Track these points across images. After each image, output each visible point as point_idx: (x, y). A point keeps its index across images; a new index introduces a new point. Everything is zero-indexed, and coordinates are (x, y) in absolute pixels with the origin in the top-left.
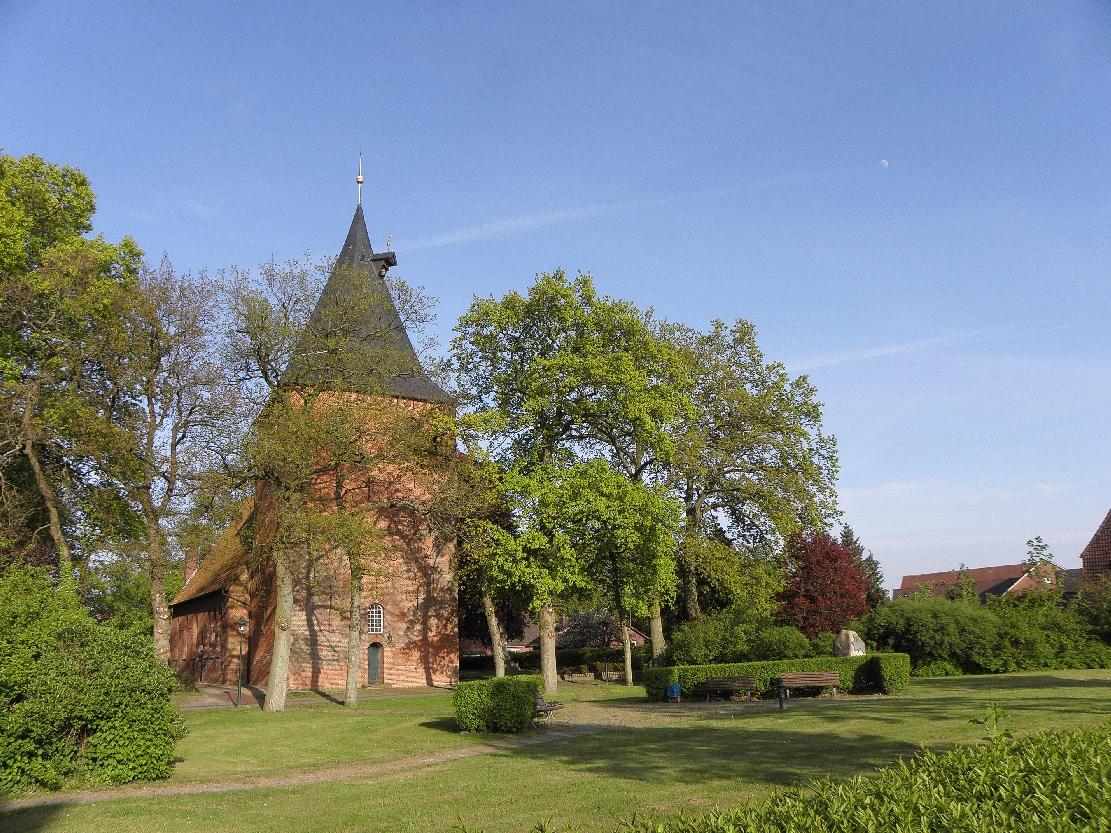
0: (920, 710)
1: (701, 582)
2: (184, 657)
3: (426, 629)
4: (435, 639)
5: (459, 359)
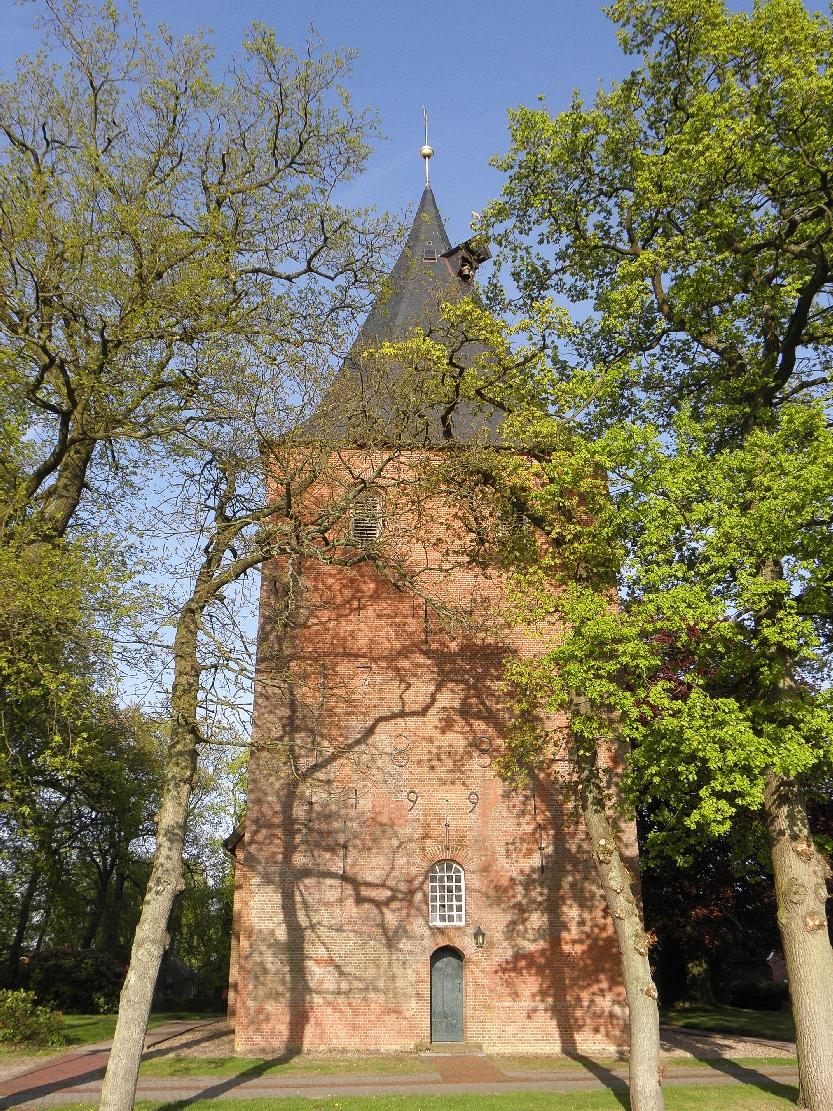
4: (579, 948)
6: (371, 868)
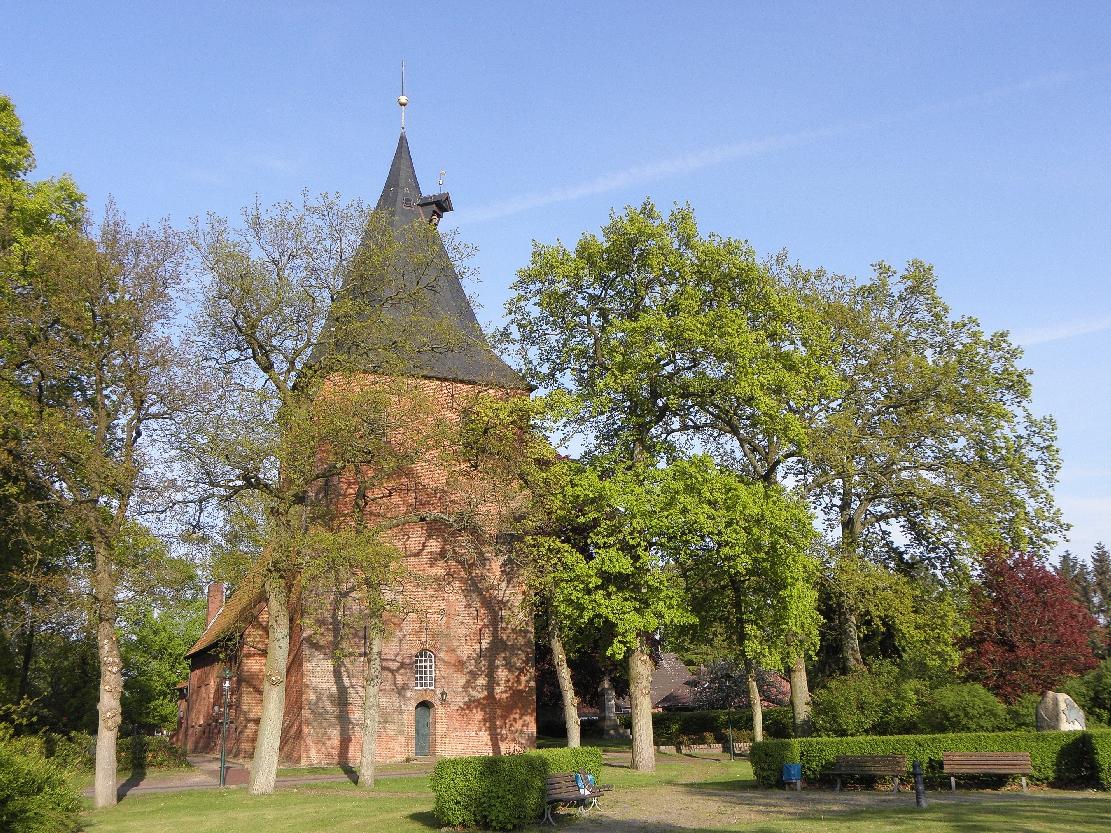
0: (1036, 817)
1: (866, 620)
2: (202, 722)
3: (492, 682)
4: (504, 696)
5: (520, 326)
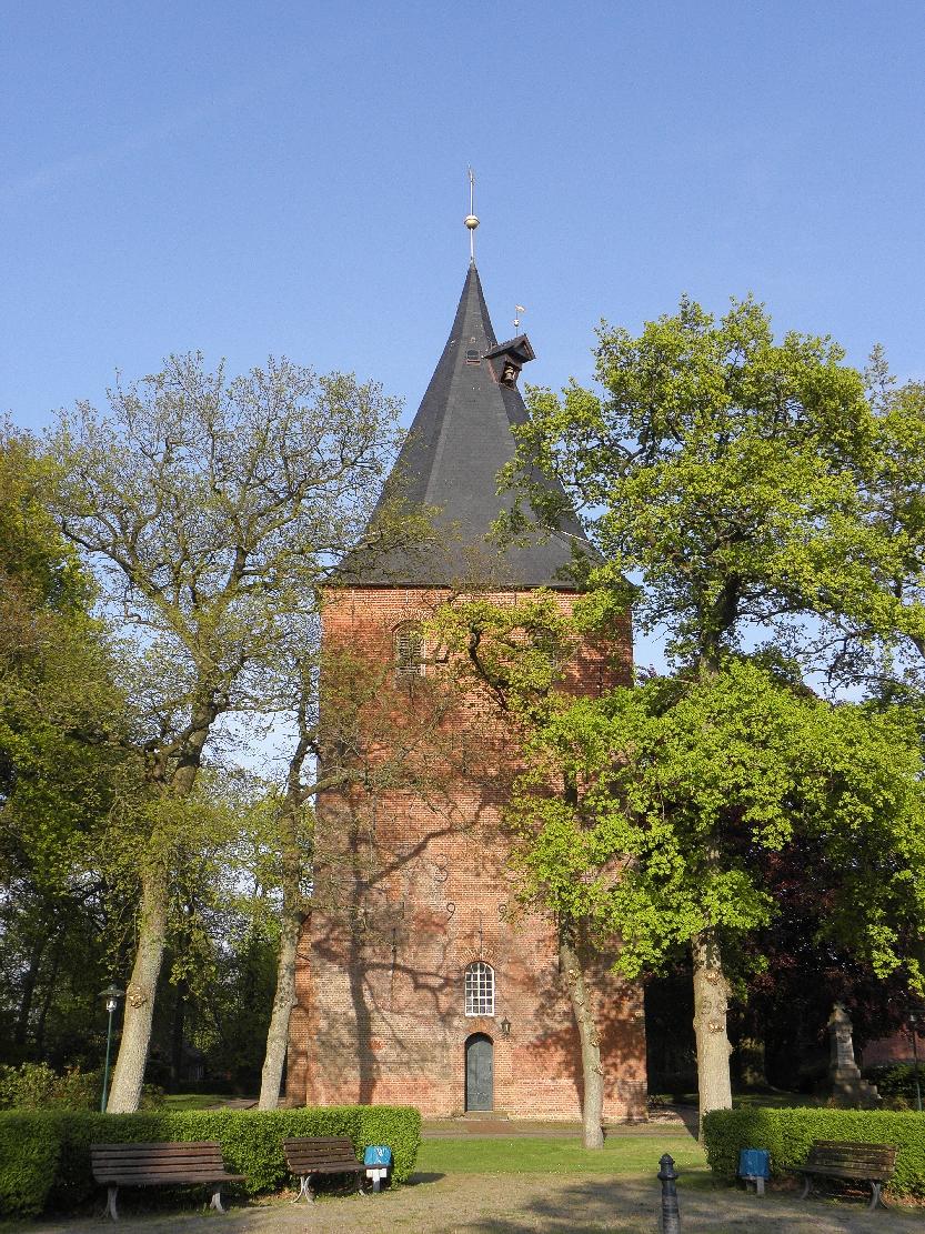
6: (430, 959)
